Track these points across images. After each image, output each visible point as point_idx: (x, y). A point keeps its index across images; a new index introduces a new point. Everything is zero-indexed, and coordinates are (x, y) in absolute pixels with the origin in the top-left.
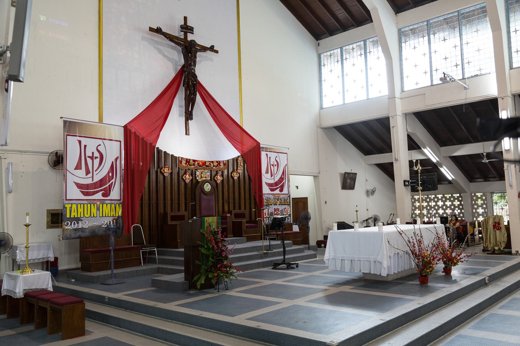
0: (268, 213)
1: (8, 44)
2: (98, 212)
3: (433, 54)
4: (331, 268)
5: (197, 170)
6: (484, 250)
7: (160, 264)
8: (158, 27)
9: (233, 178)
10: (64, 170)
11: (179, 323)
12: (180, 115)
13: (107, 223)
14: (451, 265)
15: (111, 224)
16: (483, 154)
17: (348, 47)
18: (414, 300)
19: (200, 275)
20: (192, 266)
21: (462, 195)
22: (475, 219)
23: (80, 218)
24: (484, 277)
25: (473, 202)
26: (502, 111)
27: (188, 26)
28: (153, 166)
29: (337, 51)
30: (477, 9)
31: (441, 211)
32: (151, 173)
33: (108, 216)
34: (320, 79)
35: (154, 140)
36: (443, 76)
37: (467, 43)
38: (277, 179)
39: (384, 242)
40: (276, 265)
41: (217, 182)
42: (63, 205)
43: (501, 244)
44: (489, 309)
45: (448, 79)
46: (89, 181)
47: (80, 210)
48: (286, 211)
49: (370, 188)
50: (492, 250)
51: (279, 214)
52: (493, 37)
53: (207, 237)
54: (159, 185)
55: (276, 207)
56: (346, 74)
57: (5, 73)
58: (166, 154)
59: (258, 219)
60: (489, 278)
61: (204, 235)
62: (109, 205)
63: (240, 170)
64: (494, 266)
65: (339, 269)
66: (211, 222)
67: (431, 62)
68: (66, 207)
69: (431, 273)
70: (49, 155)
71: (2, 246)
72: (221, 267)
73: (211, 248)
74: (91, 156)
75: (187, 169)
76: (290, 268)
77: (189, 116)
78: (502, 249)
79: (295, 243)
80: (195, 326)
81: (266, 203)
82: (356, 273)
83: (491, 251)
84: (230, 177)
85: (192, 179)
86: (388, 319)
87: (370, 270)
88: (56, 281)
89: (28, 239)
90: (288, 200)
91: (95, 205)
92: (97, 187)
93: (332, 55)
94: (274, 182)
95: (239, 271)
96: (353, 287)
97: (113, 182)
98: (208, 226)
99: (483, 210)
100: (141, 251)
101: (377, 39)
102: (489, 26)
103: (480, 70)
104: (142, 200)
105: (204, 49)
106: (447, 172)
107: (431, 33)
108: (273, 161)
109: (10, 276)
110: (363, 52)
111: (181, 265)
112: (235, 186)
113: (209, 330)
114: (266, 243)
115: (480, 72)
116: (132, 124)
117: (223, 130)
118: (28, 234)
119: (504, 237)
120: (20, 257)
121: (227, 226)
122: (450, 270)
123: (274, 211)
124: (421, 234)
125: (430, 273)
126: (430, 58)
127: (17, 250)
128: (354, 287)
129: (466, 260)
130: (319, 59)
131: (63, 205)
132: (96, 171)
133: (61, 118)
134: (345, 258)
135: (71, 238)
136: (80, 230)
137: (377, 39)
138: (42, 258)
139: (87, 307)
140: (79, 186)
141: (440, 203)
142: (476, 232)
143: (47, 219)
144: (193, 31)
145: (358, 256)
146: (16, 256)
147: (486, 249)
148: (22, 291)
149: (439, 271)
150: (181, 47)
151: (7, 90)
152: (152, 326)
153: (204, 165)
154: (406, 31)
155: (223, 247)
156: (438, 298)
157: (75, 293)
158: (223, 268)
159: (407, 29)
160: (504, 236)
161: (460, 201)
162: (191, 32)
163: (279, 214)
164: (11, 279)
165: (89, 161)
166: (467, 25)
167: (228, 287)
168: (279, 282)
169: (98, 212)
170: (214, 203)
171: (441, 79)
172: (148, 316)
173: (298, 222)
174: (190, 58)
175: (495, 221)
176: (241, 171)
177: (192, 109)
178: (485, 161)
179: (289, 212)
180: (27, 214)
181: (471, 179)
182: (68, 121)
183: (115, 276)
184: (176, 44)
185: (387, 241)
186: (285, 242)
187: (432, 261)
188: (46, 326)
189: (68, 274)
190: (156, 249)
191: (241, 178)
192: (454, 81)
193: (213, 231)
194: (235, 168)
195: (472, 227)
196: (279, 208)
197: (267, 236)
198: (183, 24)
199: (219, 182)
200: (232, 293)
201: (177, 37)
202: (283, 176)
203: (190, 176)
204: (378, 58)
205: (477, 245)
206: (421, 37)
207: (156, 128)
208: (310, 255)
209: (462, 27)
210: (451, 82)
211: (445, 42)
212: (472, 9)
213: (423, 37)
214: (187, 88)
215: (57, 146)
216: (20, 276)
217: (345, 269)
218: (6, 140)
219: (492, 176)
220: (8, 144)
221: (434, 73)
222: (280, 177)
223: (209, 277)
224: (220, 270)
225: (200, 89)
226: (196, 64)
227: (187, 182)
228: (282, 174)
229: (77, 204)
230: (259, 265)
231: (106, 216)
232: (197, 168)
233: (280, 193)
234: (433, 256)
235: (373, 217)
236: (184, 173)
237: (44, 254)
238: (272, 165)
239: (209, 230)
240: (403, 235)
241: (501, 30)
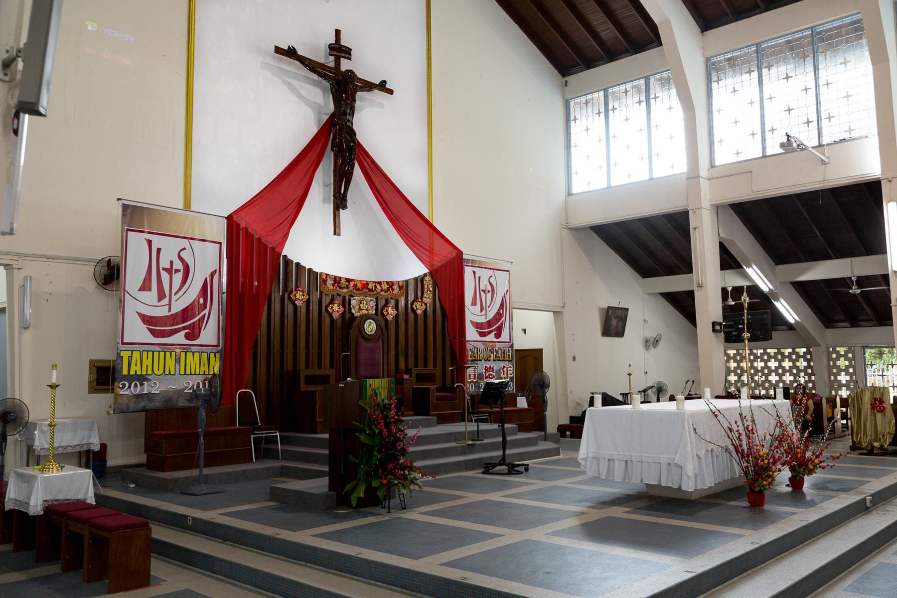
0: (475, 375)
1: (19, 44)
2: (177, 366)
3: (766, 103)
4: (591, 473)
5: (353, 297)
6: (854, 447)
7: (285, 459)
8: (291, 46)
9: (414, 311)
10: (121, 291)
11: (319, 567)
12: (325, 201)
13: (193, 386)
14: (803, 474)
15: (201, 387)
16: (850, 278)
17: (618, 89)
18: (742, 536)
19: (357, 482)
20: (342, 466)
21: (811, 349)
22: (833, 393)
23: (146, 376)
24: (864, 496)
25: (831, 363)
26: (889, 202)
27: (342, 46)
28: (276, 288)
29: (597, 95)
30: (846, 25)
31: (788, 378)
32: (273, 300)
33: (195, 374)
34: (567, 143)
35: (278, 243)
36: (785, 140)
37: (828, 84)
38: (491, 315)
39: (687, 430)
40: (488, 467)
41: (387, 319)
42: (117, 352)
43: (885, 437)
44: (876, 555)
45: (795, 145)
46: (162, 312)
47: (147, 362)
48: (505, 372)
49: (651, 335)
50: (869, 448)
51: (494, 377)
52: (874, 73)
53: (370, 415)
54: (286, 321)
55: (488, 364)
56: (613, 136)
57: (12, 98)
58: (299, 266)
59: (457, 386)
60: (873, 498)
61: (366, 410)
62: (197, 355)
63: (428, 300)
64: (878, 475)
65: (604, 477)
66: (378, 388)
67: (764, 116)
68: (122, 357)
69: (771, 486)
70: (95, 264)
71: (10, 422)
72: (395, 468)
73: (377, 433)
74: (169, 267)
75: (335, 294)
76: (514, 472)
77: (340, 202)
78: (886, 446)
79: (522, 429)
80: (347, 575)
81: (471, 357)
82: (634, 484)
83: (867, 450)
84: (409, 310)
85: (344, 313)
86: (700, 570)
87: (660, 480)
88: (101, 486)
89: (54, 410)
90: (509, 352)
91: (173, 354)
92: (177, 322)
93: (589, 102)
94: (486, 321)
95: (426, 475)
96: (629, 509)
97: (205, 314)
98: (372, 395)
99: (848, 378)
100: (252, 436)
101: (669, 76)
102: (867, 53)
103: (850, 130)
104: (255, 346)
105: (369, 86)
106: (787, 310)
107: (764, 65)
108: (484, 284)
109: (20, 476)
110: (643, 98)
111: (323, 464)
112: (419, 326)
113: (374, 582)
114: (472, 427)
115: (850, 134)
116: (241, 214)
117: (399, 227)
118: (54, 402)
119: (890, 425)
120: (40, 441)
121: (403, 396)
122: (801, 482)
123: (484, 371)
124: (752, 417)
125: (768, 487)
126: (762, 108)
127: (35, 430)
128: (630, 509)
129: (831, 464)
130: (567, 109)
131: (117, 352)
132: (176, 294)
133: (118, 199)
134: (615, 457)
135: (130, 411)
136: (145, 397)
137: (669, 76)
138: (79, 445)
139: (154, 535)
140: (147, 320)
141: (787, 364)
142: (837, 415)
143: (90, 377)
144: (351, 55)
145: (639, 454)
146: (33, 440)
147: (858, 446)
148: (41, 503)
149: (781, 483)
150: (329, 82)
151: (16, 132)
152: (269, 572)
153: (364, 288)
154: (720, 62)
155: (399, 433)
156: (786, 532)
157: (135, 508)
158: (397, 470)
159: (721, 58)
160: (890, 423)
161: (808, 361)
162: (347, 56)
163: (494, 377)
164: (22, 482)
165: (165, 276)
166: (828, 53)
167: (406, 504)
168: (496, 497)
169: (177, 366)
170: (381, 355)
171: (782, 145)
172: (264, 555)
173: (527, 392)
174: (344, 100)
175: (873, 395)
176: (428, 300)
177: (346, 189)
178: (855, 290)
179: (511, 374)
180: (53, 366)
181: (828, 321)
182: (130, 205)
183: (207, 479)
184: (321, 77)
185: (692, 428)
186: (506, 426)
187: (771, 465)
188: (82, 568)
189: (124, 474)
190: (278, 434)
191: (428, 312)
192: (805, 149)
193: (381, 405)
194: (419, 295)
195: (829, 406)
196: (493, 367)
197: (472, 416)
198: (334, 43)
199: (390, 318)
200: (412, 515)
201: (323, 64)
202: (501, 310)
203: (341, 307)
204: (670, 108)
205: (838, 438)
206: (746, 73)
207: (283, 222)
208: (548, 450)
209: (818, 55)
210: (799, 150)
211: (787, 81)
212: (836, 24)
213: (750, 72)
214: (339, 152)
215: (109, 250)
216: (37, 477)
217: (614, 476)
218: (12, 224)
219: (864, 317)
220: (14, 232)
221: (768, 135)
222: (497, 313)
223: (373, 486)
224: (392, 474)
225: (361, 156)
226: (355, 112)
227: (334, 317)
228: (500, 307)
229: (141, 351)
230: (458, 466)
231: (191, 374)
232: (353, 292)
233: (496, 340)
234: (774, 457)
235: (656, 385)
236: (329, 300)
237: (83, 439)
238: (484, 291)
239: (374, 402)
240: (720, 417)
241: (889, 61)
